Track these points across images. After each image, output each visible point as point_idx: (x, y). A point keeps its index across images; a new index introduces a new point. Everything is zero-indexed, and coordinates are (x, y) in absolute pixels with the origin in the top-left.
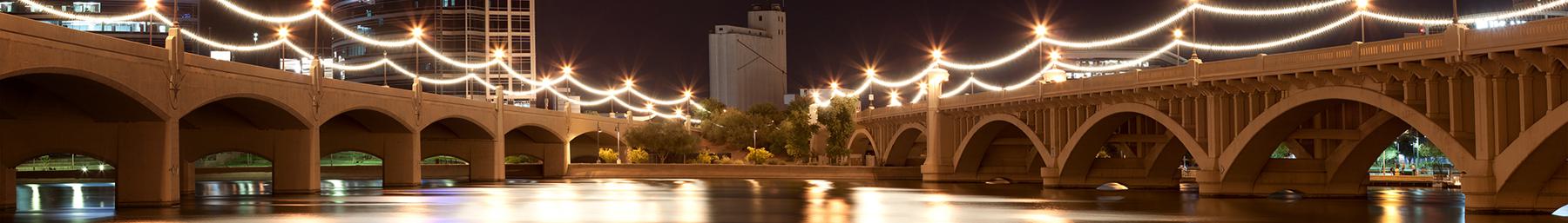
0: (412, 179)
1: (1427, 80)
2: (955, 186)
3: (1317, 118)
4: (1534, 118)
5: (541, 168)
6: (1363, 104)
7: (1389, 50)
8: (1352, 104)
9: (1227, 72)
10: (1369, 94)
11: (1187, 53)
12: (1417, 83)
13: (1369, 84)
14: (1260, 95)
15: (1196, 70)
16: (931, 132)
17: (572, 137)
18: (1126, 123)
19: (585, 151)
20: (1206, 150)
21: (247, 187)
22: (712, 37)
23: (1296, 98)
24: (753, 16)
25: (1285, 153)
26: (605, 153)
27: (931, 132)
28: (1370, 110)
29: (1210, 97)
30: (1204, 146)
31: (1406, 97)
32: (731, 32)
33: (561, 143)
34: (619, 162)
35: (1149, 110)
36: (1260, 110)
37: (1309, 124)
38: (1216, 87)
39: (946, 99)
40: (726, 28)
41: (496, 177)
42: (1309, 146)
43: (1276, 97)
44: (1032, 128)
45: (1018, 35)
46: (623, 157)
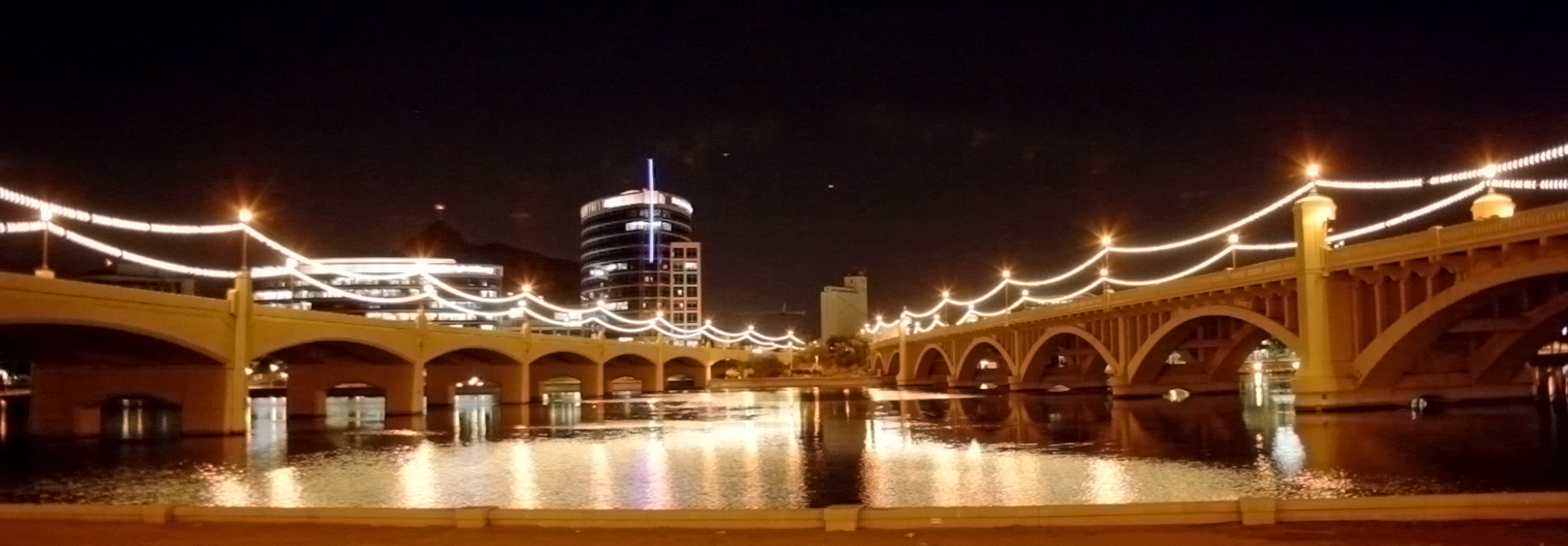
0: (221, 417)
1: (1401, 282)
2: (915, 388)
3: (1200, 331)
4: (1389, 321)
5: (692, 382)
6: (1235, 319)
7: (1256, 273)
8: (1225, 319)
9: (1131, 300)
10: (1241, 311)
11: (1029, 304)
12: (1277, 300)
13: (1239, 302)
14: (1155, 316)
15: (1110, 301)
16: (902, 351)
17: (712, 363)
18: (1067, 341)
19: (719, 371)
20: (1489, 334)
21: (1418, 403)
22: (823, 294)
23: (1182, 316)
24: (847, 279)
25: (1174, 358)
26: (730, 372)
27: (902, 351)
28: (1239, 323)
29: (1016, 333)
30: (1116, 356)
31: (1268, 310)
32: (834, 290)
33: (703, 367)
34: (740, 378)
35: (1076, 330)
36: (1155, 327)
37: (1194, 336)
38: (1125, 310)
39: (931, 331)
40: (831, 288)
41: (657, 390)
42: (1194, 353)
43: (1167, 316)
44: (1098, 337)
45: (783, 333)
46: (742, 375)
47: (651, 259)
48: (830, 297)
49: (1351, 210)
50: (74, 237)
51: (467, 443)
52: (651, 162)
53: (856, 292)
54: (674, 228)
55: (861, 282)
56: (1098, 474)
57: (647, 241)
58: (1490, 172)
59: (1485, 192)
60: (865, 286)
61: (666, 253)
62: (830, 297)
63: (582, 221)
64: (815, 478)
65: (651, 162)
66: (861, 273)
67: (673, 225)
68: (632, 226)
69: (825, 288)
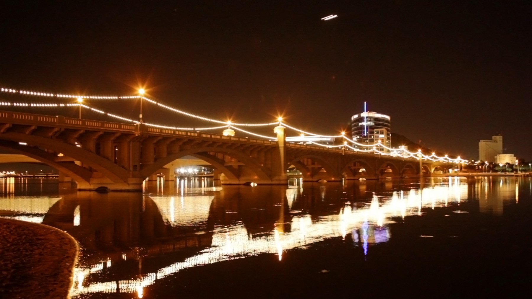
22: (480, 143)
24: (493, 137)
32: (484, 142)
40: (483, 141)
47: (365, 135)
48: (483, 144)
49: (270, 131)
50: (218, 122)
51: (287, 233)
52: (365, 103)
53: (497, 142)
54: (375, 124)
55: (499, 138)
56: (237, 237)
57: (364, 128)
58: (229, 123)
59: (227, 128)
60: (501, 139)
61: (372, 132)
62: (483, 144)
63: (352, 121)
64: (97, 260)
65: (365, 103)
66: (500, 135)
67: (375, 123)
68: (360, 124)
69: (481, 141)
